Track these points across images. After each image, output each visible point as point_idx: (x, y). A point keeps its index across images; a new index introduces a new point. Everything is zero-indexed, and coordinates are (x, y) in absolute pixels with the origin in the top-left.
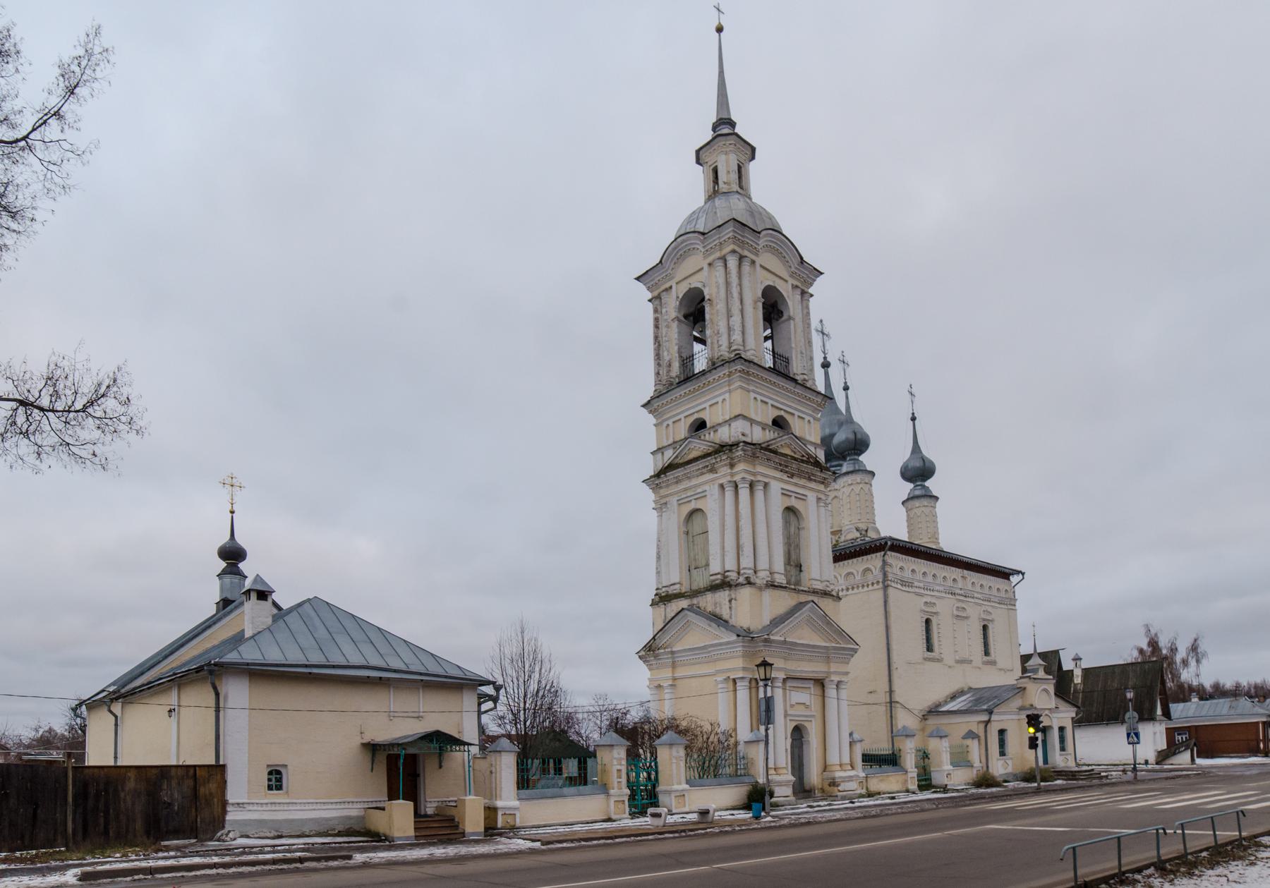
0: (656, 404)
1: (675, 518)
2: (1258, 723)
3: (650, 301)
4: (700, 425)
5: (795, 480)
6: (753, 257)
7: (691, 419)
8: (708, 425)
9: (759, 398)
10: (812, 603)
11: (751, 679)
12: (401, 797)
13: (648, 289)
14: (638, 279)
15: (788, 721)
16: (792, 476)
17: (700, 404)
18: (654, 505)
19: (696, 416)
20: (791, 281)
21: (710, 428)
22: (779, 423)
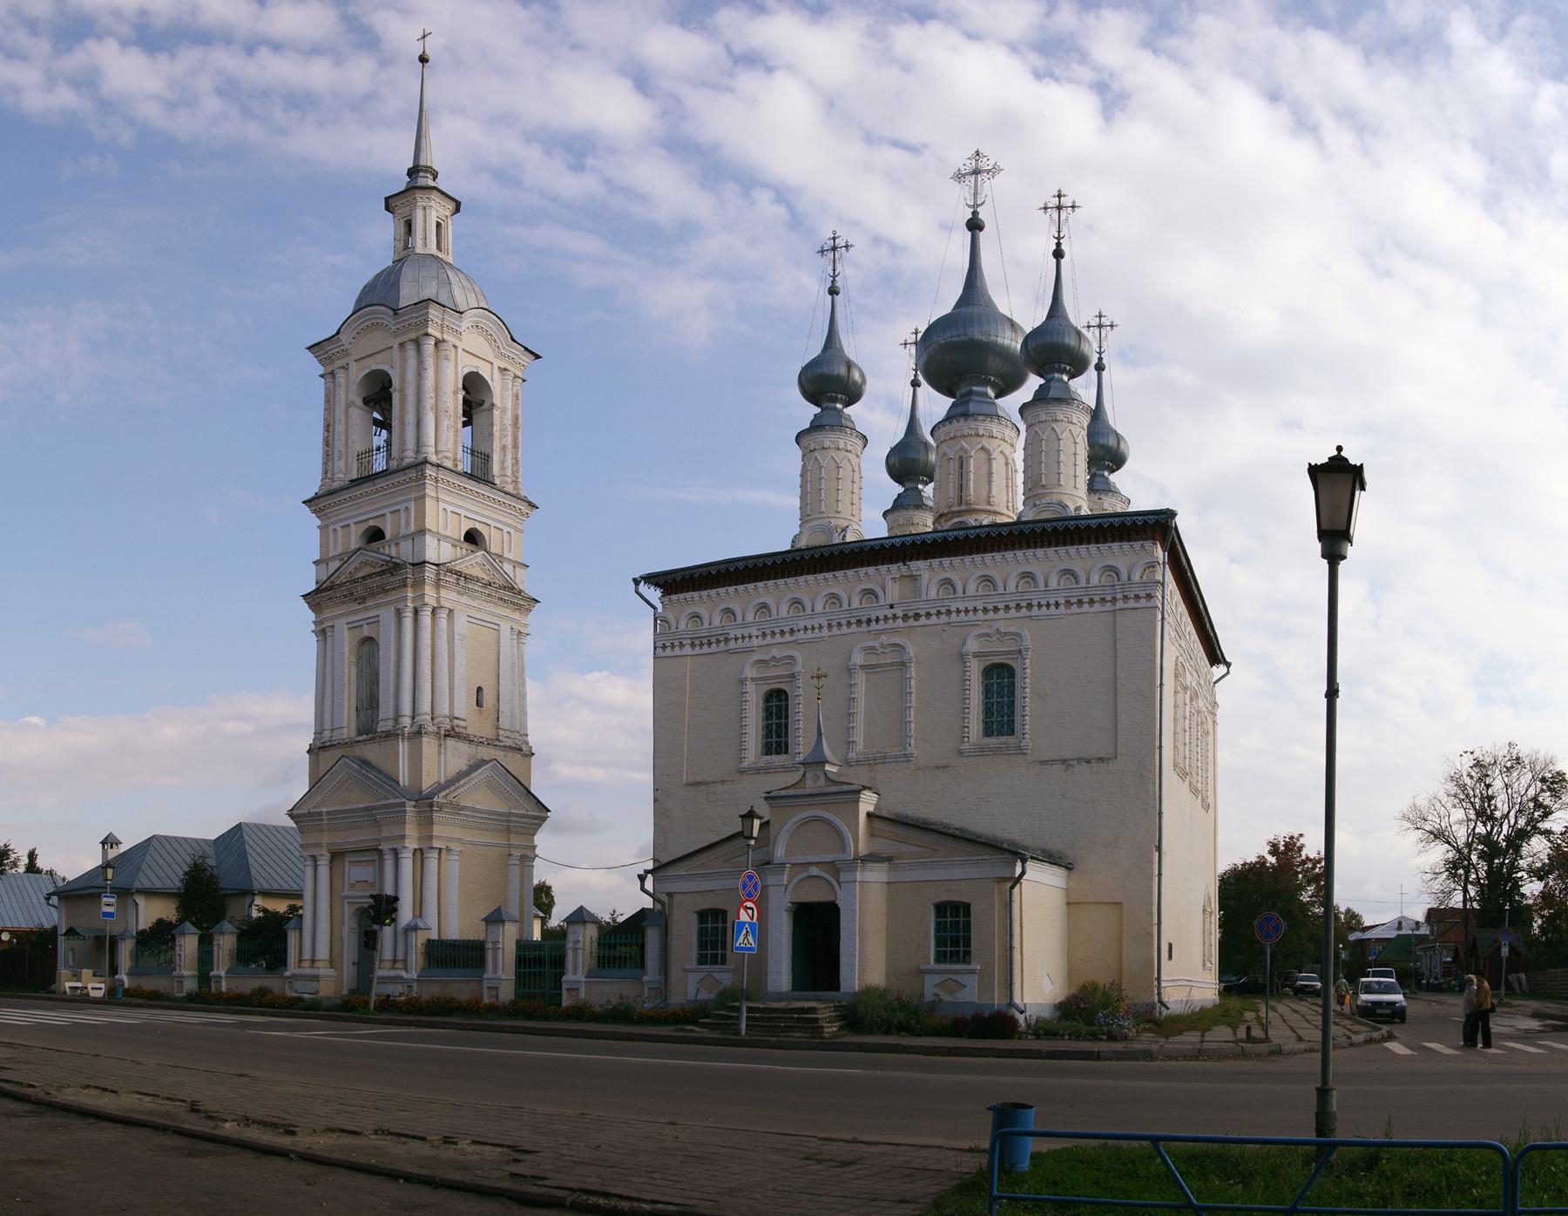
0: (322, 503)
1: (345, 641)
2: (711, 964)
3: (322, 376)
4: (376, 535)
5: (369, 603)
6: (423, 332)
7: (364, 527)
8: (388, 535)
9: (449, 508)
10: (495, 762)
11: (415, 850)
12: (560, 942)
13: (320, 361)
14: (309, 348)
15: (346, 903)
16: (364, 598)
17: (395, 504)
18: (313, 627)
19: (371, 523)
20: (498, 363)
21: (391, 540)
22: (472, 538)
